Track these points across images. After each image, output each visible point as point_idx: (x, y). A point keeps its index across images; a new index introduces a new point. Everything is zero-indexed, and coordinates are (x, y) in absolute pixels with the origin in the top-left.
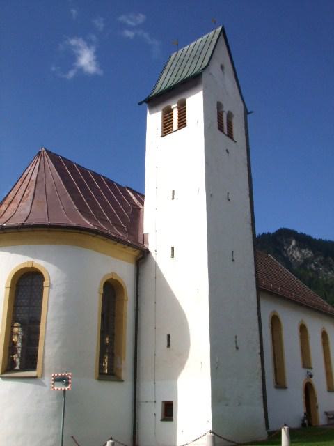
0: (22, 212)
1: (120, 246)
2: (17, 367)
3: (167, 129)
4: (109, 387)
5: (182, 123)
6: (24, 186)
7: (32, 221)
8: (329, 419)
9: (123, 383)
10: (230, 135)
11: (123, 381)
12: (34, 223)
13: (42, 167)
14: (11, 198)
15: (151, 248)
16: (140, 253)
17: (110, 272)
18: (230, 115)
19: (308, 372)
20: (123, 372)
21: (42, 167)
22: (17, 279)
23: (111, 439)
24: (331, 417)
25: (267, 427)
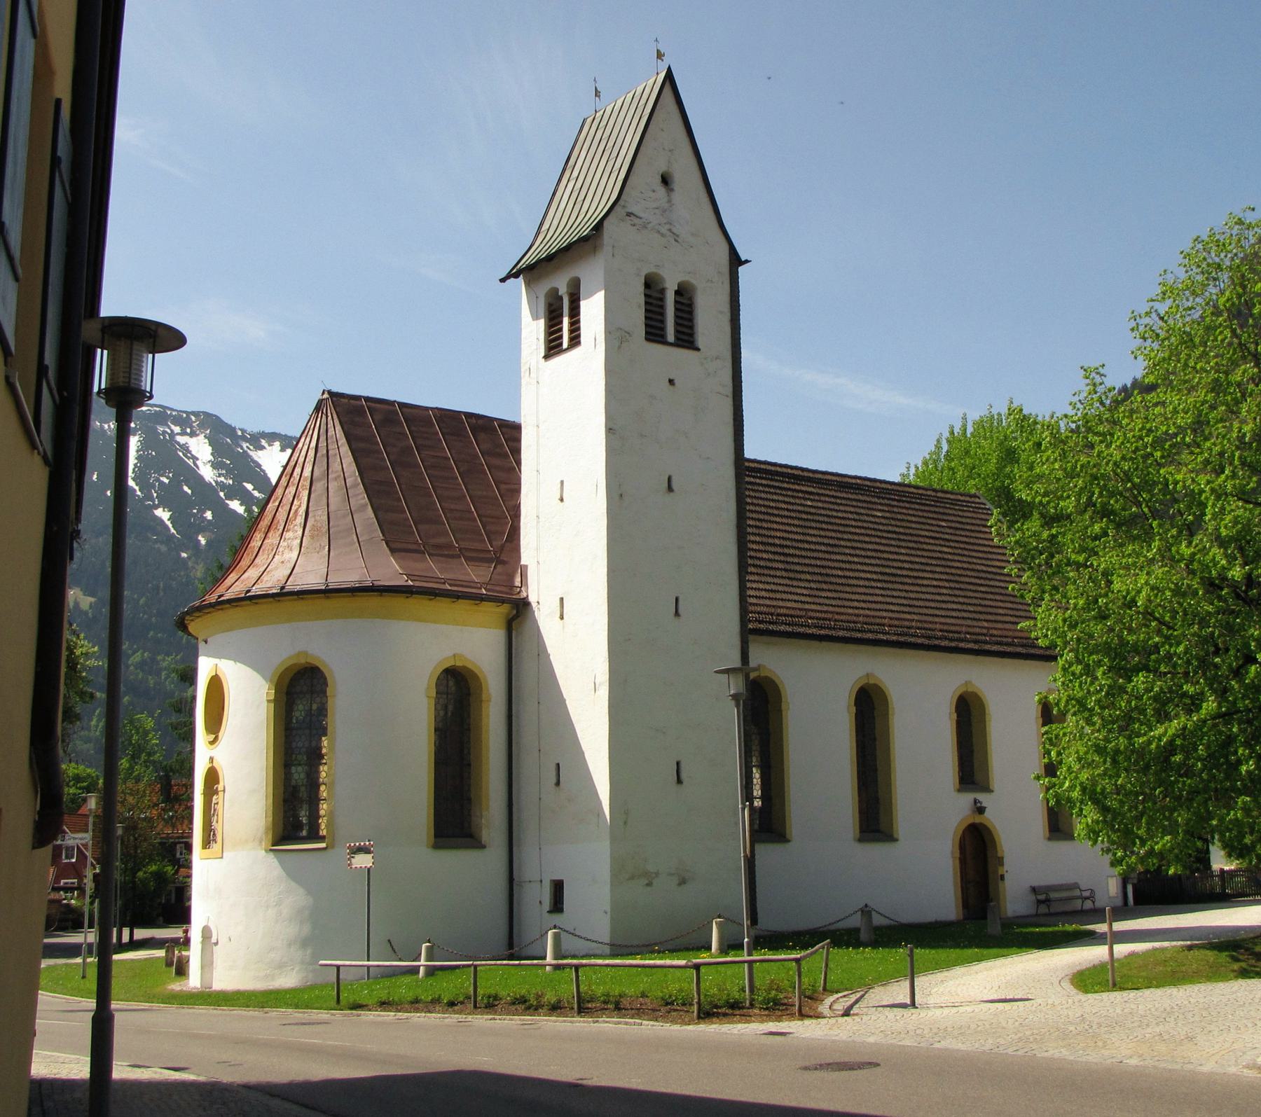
0: (320, 512)
1: (463, 605)
2: (304, 833)
3: (553, 348)
4: (456, 860)
5: (575, 341)
6: (292, 490)
7: (297, 583)
8: (1039, 902)
9: (486, 851)
10: (686, 339)
11: (484, 847)
12: (298, 588)
13: (323, 444)
14: (270, 518)
15: (532, 599)
16: (513, 608)
17: (449, 653)
18: (685, 295)
19: (976, 801)
20: (484, 832)
21: (323, 444)
22: (287, 681)
23: (429, 942)
24: (1042, 897)
25: (754, 919)
